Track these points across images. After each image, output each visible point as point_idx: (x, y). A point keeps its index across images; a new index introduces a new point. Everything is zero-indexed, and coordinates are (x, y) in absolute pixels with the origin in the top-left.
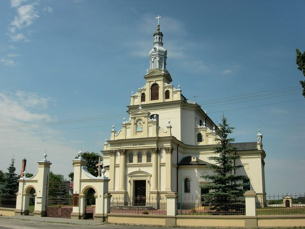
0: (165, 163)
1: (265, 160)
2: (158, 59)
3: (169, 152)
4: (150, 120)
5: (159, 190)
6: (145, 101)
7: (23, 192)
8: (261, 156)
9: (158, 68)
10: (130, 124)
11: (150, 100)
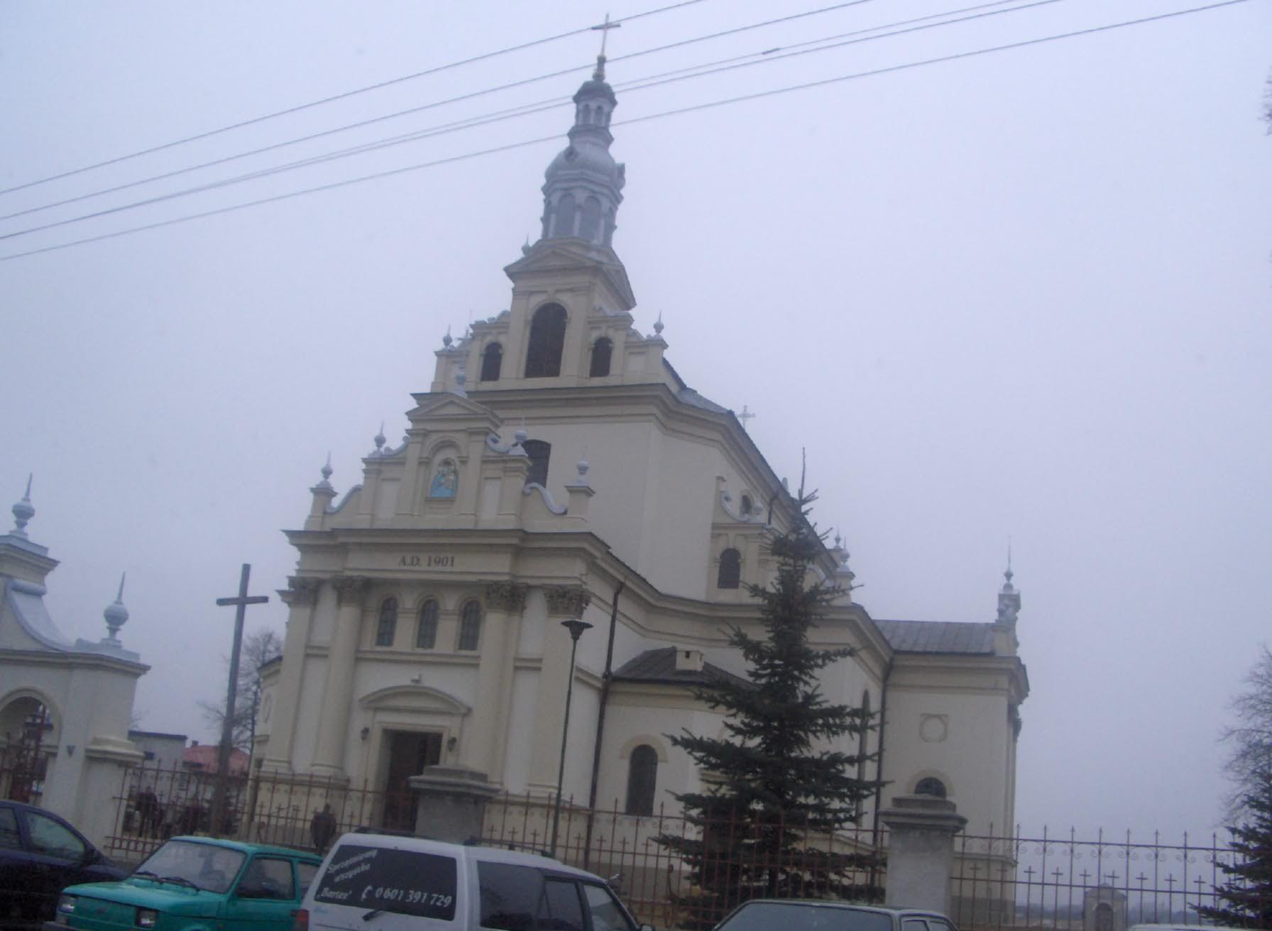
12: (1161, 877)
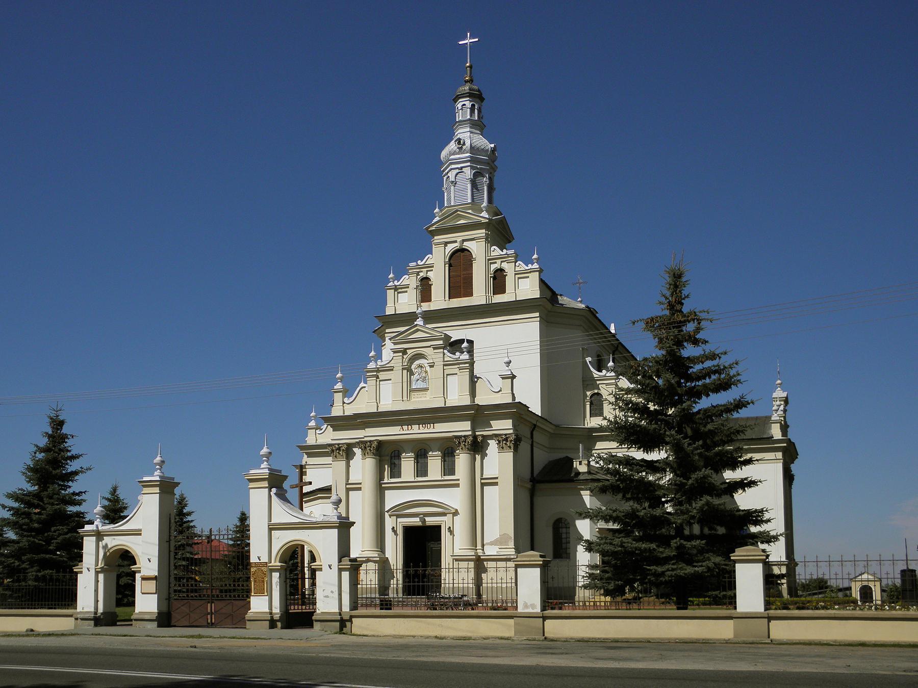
0: (497, 478)
1: (794, 467)
2: (468, 173)
3: (510, 447)
4: (449, 356)
5: (480, 552)
6: (430, 300)
7: (97, 564)
8: (784, 456)
9: (469, 201)
10: (391, 369)
11: (447, 298)
12: (883, 573)
